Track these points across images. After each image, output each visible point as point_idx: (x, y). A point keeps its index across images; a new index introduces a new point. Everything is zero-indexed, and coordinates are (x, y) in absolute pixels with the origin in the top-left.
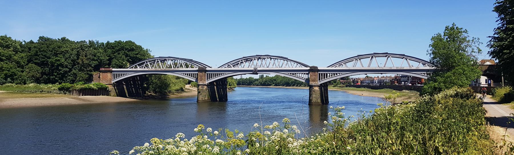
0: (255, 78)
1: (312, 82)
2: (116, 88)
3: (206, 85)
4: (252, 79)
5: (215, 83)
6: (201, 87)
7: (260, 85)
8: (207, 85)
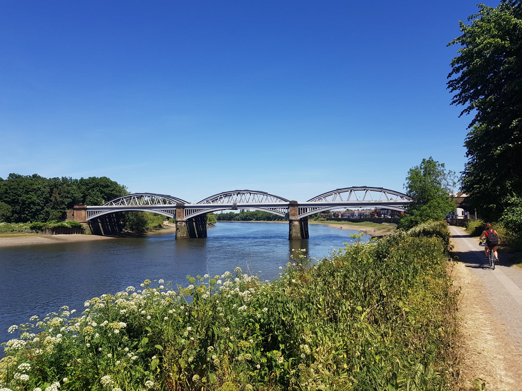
1: (292, 217)
2: (91, 226)
5: (194, 219)
6: (180, 224)
7: (240, 220)
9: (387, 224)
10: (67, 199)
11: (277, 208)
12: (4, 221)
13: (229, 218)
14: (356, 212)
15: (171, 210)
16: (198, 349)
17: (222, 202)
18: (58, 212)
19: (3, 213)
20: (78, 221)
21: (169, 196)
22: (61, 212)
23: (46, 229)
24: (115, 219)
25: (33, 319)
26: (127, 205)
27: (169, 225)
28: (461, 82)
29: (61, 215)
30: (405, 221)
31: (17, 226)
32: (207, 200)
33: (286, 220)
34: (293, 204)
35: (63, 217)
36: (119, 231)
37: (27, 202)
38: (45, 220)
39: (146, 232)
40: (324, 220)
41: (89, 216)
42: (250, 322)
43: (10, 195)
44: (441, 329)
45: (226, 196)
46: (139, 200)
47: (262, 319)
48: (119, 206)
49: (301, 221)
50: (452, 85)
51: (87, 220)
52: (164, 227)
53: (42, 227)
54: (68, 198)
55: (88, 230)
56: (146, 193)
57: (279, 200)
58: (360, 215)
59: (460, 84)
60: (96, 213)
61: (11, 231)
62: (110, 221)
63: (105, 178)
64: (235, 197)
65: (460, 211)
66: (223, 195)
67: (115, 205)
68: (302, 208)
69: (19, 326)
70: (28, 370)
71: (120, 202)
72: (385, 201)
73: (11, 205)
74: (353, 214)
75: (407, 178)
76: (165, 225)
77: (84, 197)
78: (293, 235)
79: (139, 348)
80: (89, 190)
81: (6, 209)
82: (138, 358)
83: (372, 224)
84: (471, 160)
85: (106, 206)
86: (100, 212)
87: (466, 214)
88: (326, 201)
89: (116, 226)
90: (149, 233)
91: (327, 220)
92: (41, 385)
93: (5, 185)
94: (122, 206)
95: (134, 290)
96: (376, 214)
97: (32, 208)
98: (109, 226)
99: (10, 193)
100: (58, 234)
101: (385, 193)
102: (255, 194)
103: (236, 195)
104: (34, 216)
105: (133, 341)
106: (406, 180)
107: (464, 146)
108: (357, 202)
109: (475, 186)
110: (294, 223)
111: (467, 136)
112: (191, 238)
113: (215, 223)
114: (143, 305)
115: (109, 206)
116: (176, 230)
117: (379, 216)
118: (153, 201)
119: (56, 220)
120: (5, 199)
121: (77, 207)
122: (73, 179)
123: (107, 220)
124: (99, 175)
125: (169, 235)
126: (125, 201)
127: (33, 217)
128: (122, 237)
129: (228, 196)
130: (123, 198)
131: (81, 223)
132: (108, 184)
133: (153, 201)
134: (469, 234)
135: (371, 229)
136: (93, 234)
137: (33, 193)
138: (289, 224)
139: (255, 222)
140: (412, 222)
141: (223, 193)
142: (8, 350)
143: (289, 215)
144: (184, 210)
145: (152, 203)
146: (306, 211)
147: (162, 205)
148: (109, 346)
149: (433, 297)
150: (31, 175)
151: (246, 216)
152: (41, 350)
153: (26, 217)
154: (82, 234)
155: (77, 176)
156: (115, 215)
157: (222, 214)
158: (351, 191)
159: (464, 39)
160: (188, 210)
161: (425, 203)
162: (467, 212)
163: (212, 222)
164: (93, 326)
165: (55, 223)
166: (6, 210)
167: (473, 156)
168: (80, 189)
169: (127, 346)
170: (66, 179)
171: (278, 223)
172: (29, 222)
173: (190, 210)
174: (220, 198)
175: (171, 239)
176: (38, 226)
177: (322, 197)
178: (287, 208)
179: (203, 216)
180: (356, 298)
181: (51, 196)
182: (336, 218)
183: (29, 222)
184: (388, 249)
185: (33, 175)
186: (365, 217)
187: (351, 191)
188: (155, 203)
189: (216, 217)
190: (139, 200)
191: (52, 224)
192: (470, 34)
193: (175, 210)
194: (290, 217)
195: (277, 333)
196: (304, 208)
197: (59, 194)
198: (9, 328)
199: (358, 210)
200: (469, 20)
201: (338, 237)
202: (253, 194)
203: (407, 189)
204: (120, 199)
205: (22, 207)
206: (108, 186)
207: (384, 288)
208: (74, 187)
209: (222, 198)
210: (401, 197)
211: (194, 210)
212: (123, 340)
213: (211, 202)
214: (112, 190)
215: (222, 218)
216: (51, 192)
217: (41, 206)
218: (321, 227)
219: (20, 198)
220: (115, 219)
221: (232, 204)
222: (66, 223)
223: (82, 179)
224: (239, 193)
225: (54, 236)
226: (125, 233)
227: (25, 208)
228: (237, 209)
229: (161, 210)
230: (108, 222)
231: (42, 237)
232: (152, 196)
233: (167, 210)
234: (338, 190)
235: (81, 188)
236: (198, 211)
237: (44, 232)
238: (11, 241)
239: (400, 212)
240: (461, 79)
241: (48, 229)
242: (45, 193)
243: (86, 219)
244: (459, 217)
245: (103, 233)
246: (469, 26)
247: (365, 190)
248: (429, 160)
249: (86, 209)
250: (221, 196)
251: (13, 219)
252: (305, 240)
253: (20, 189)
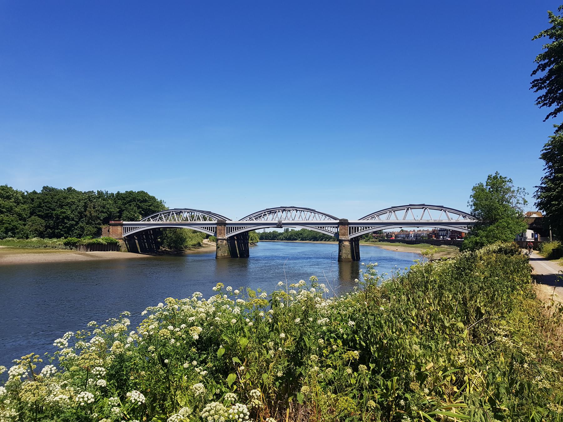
0: (279, 232)
1: (342, 237)
2: (127, 242)
5: (235, 237)
6: (221, 242)
9: (446, 246)
10: (102, 214)
11: (326, 227)
12: (36, 236)
13: (273, 237)
14: (411, 233)
15: (212, 227)
16: (286, 364)
17: (266, 219)
18: (93, 227)
19: (36, 227)
20: (113, 238)
21: (210, 212)
22: (96, 227)
23: (80, 245)
24: (152, 236)
25: (91, 325)
26: (165, 221)
27: (209, 243)
28: (548, 82)
29: (95, 231)
30: (469, 243)
31: (51, 242)
32: (250, 217)
33: (334, 241)
34: (343, 223)
35: (98, 233)
36: (156, 248)
37: (61, 217)
38: (80, 236)
39: (184, 251)
40: (376, 242)
41: (126, 232)
42: (331, 337)
43: (44, 209)
44: (552, 352)
45: (270, 213)
46: (178, 216)
47: (345, 335)
48: (157, 222)
49: (351, 241)
50: (537, 84)
51: (123, 236)
52: (204, 246)
53: (76, 243)
54: (104, 213)
55: (124, 247)
56: (185, 209)
57: (328, 217)
58: (416, 237)
59: (545, 84)
60: (133, 229)
61: (44, 247)
62: (147, 238)
63: (143, 192)
64: (280, 214)
65: (529, 234)
66: (267, 212)
67: (153, 221)
68: (353, 228)
69: (76, 333)
70: (103, 375)
71: (158, 217)
72: (445, 220)
73: (44, 220)
74: (408, 235)
75: (471, 196)
76: (204, 243)
77: (121, 212)
78: (343, 256)
79: (208, 362)
80: (126, 204)
81: (39, 223)
82: (208, 374)
83: (429, 246)
84: (548, 174)
85: (143, 222)
86: (137, 228)
87: (536, 237)
88: (380, 219)
89: (153, 244)
90: (188, 252)
91: (380, 241)
92: (101, 400)
93: (38, 198)
94: (160, 222)
95: (201, 296)
96: (434, 236)
97: (67, 223)
98: (146, 244)
99: (43, 206)
100: (93, 251)
101: (445, 212)
102: (302, 211)
103: (281, 212)
104: (69, 231)
105: (201, 353)
106: (470, 198)
107: (540, 158)
108: (414, 221)
109: (553, 202)
110: (344, 243)
111: (544, 147)
112: (232, 257)
113: (257, 242)
114: (211, 313)
115: (146, 222)
116: (217, 248)
117: (437, 238)
118: (192, 217)
119: (91, 236)
120: (39, 213)
121: (113, 222)
122: (109, 193)
123: (144, 237)
124: (136, 189)
125: (206, 254)
126: (163, 217)
127: (67, 233)
128: (160, 255)
129: (272, 213)
130: (161, 214)
131: (117, 240)
132: (146, 199)
133: (192, 217)
134: (544, 257)
135: (434, 251)
136: (129, 252)
137: (67, 207)
138: (339, 244)
139: (300, 242)
140: (477, 243)
141: (267, 209)
142: (63, 359)
143: (339, 234)
144: (225, 228)
145: (191, 220)
146: (358, 231)
147: (202, 222)
148: (177, 358)
149: (529, 319)
150: (66, 188)
151: (291, 236)
152: (101, 361)
153: (60, 233)
154: (117, 251)
155: (113, 190)
157: (264, 233)
158: (408, 209)
159: (553, 31)
160: (229, 227)
161: (491, 223)
162: (537, 234)
163: (254, 241)
164: (169, 329)
165: (89, 239)
166: (39, 225)
167: (551, 169)
168: (116, 204)
169: (195, 359)
170: (102, 192)
171: (325, 244)
172: (63, 237)
173: (231, 227)
174: (264, 215)
175: (211, 258)
176: (72, 242)
177: (375, 216)
178: (336, 227)
179: (246, 234)
180: (456, 313)
181: (85, 210)
182: (390, 239)
183: (63, 237)
184: (471, 265)
185: (67, 188)
186: (421, 239)
187: (407, 209)
188: (195, 220)
189: (259, 236)
190: (178, 216)
191: (87, 240)
192: (560, 26)
193: (216, 227)
194: (340, 237)
195: (373, 348)
196: (355, 227)
197: (94, 208)
198: (65, 335)
199: (414, 231)
200: (559, 11)
201: (391, 260)
202: (300, 211)
203: (471, 208)
204: (158, 215)
205: (56, 222)
206: (145, 201)
207: (482, 304)
208: (110, 201)
209: (266, 214)
210: (464, 217)
211: (236, 228)
212: (189, 353)
213: (254, 219)
214: (150, 206)
215: (265, 237)
216: (85, 207)
217: (75, 221)
218: (373, 249)
219: (53, 212)
220: (152, 236)
221: (276, 222)
222: (101, 240)
223: (118, 193)
224: (284, 210)
225: (89, 252)
226: (163, 251)
227: (59, 223)
228: (282, 227)
229: (201, 227)
231: (76, 254)
232: (192, 212)
233: (207, 227)
234: (393, 207)
235: (118, 203)
236: (240, 229)
237: (78, 248)
238: (44, 257)
239: (460, 233)
240: (548, 78)
241: (83, 245)
242: (80, 207)
243: (122, 236)
244: (528, 239)
245: (139, 251)
246: (559, 17)
247: (423, 208)
248: (496, 176)
249: (122, 225)
250: (265, 212)
251: (46, 234)
252: (355, 262)
253: (54, 202)
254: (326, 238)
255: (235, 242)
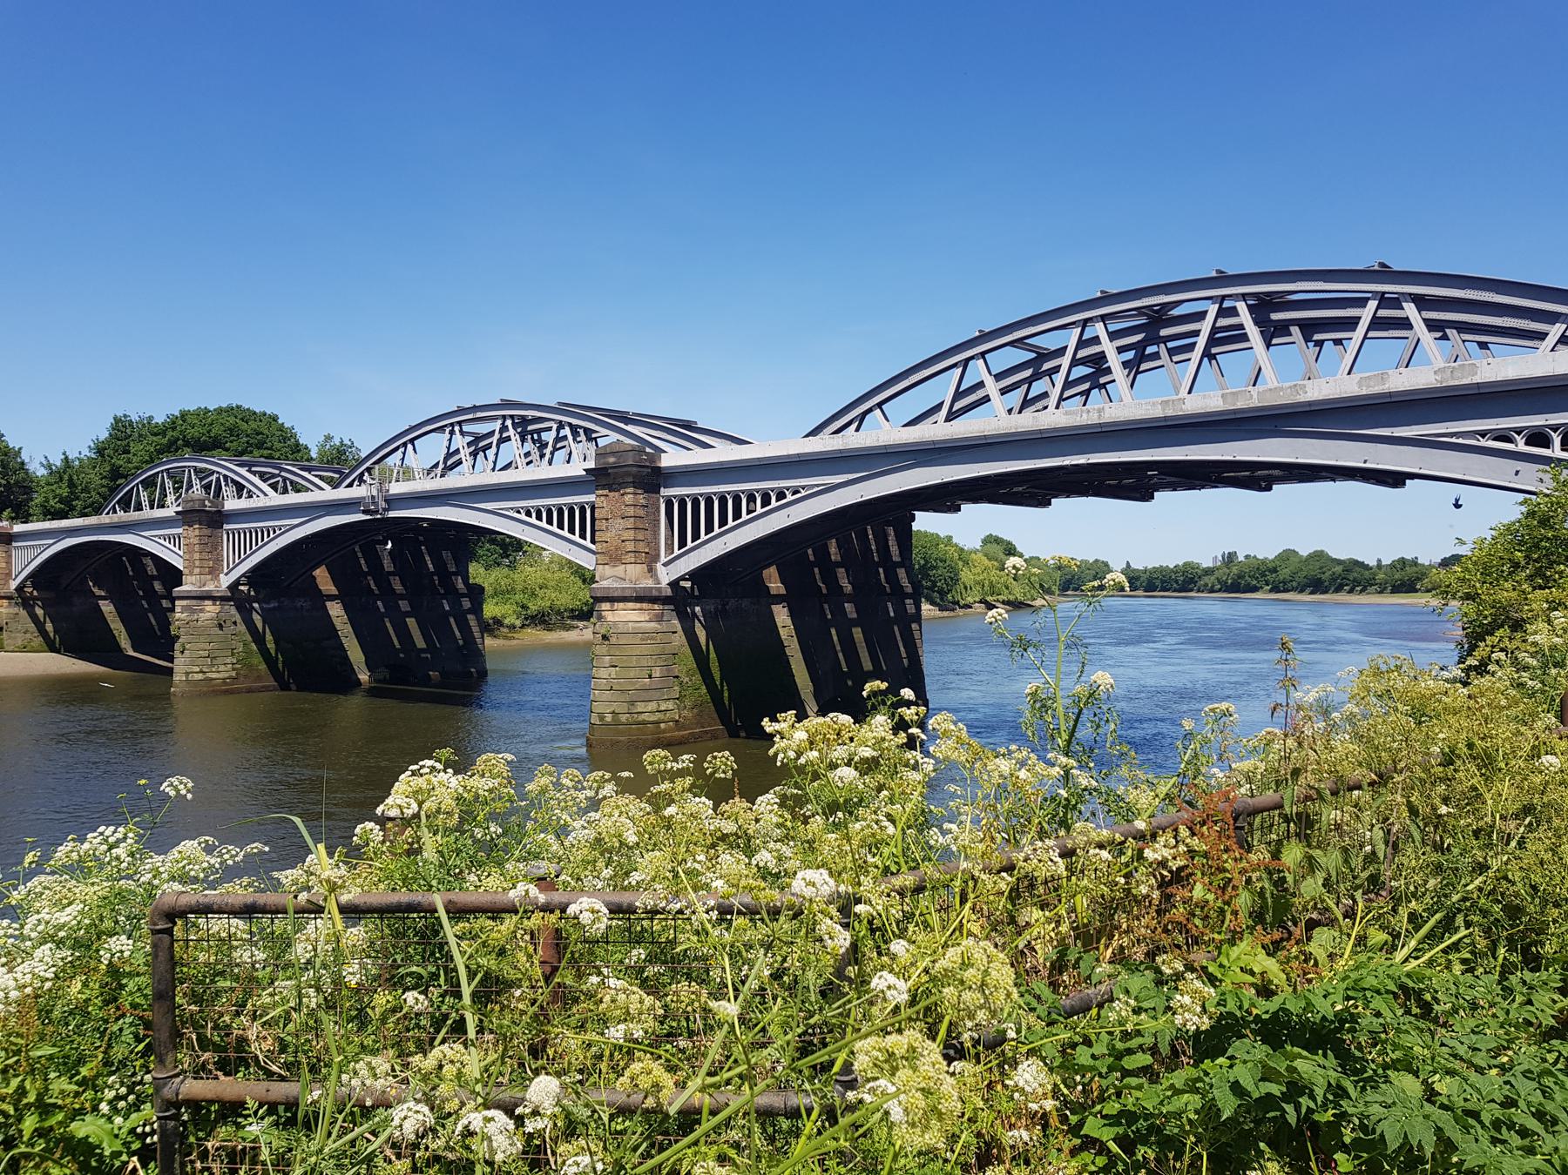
2: (257, 618)
3: (213, 598)
4: (1193, 568)
6: (185, 609)
7: (1220, 590)
8: (677, 599)
51: (666, 576)
110: (609, 616)
141: (1107, 299)
151: (1240, 576)
156: (839, 547)
230: (402, 597)
254: (1354, 580)
255: (385, 607)
